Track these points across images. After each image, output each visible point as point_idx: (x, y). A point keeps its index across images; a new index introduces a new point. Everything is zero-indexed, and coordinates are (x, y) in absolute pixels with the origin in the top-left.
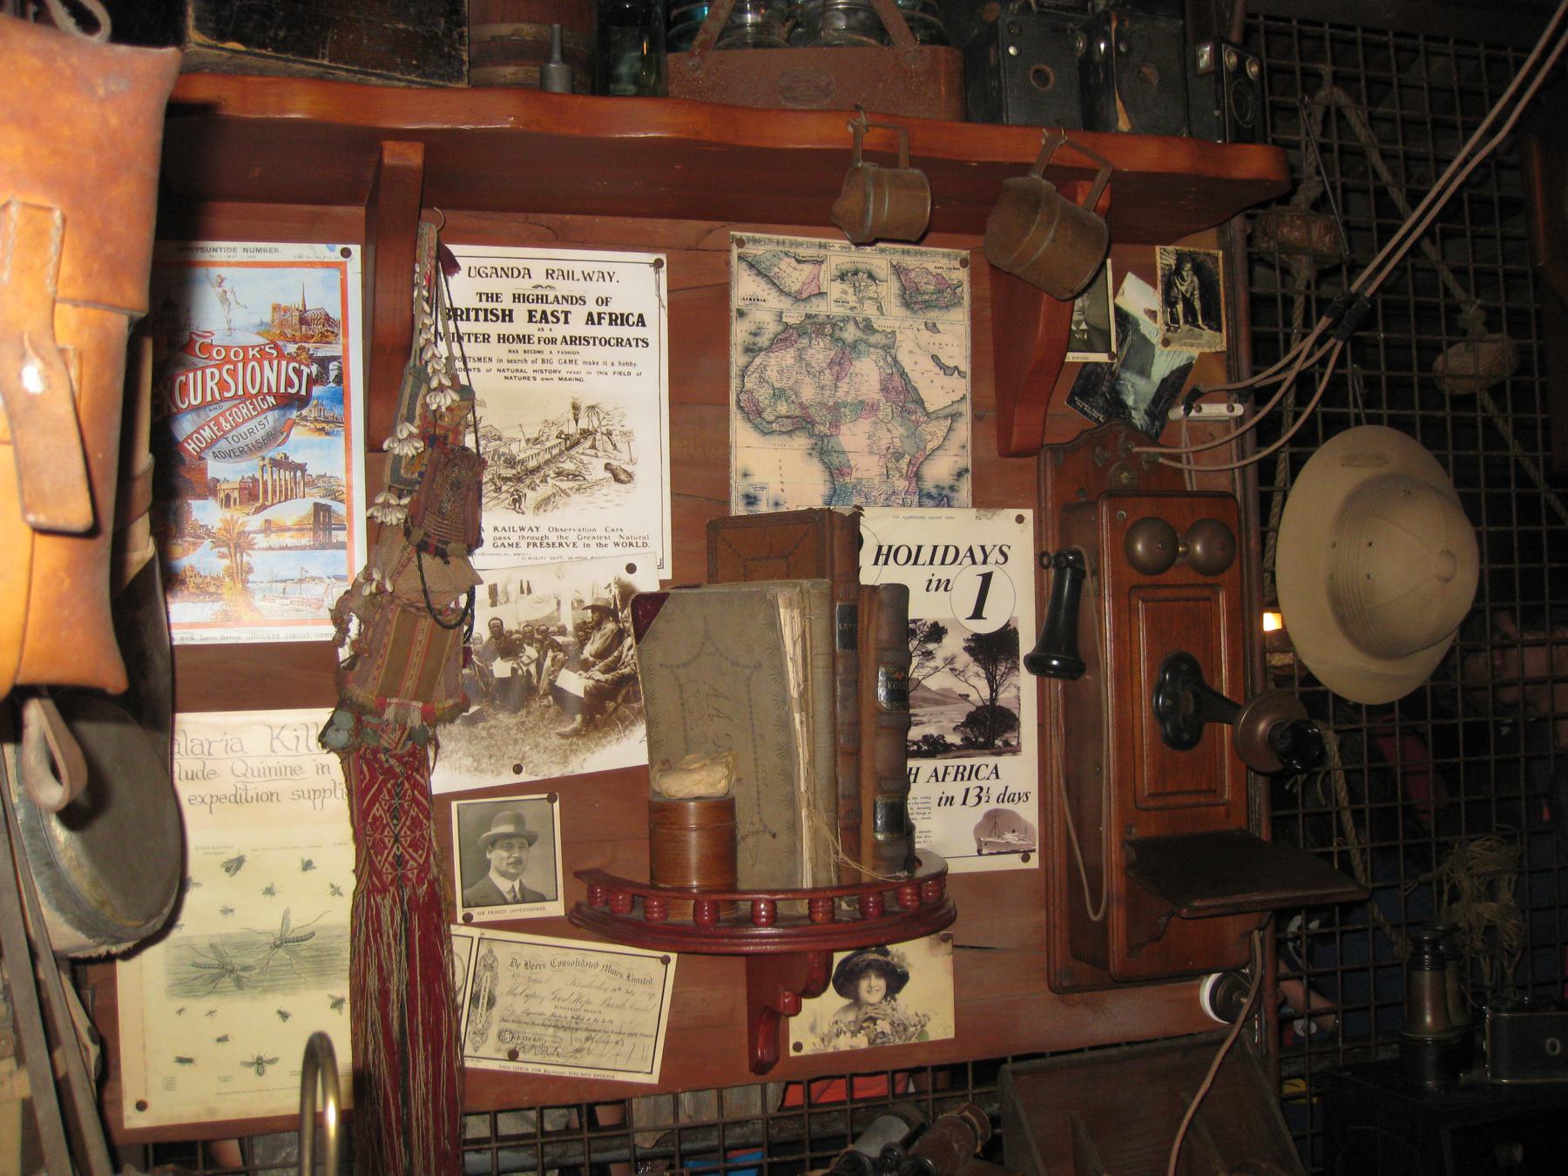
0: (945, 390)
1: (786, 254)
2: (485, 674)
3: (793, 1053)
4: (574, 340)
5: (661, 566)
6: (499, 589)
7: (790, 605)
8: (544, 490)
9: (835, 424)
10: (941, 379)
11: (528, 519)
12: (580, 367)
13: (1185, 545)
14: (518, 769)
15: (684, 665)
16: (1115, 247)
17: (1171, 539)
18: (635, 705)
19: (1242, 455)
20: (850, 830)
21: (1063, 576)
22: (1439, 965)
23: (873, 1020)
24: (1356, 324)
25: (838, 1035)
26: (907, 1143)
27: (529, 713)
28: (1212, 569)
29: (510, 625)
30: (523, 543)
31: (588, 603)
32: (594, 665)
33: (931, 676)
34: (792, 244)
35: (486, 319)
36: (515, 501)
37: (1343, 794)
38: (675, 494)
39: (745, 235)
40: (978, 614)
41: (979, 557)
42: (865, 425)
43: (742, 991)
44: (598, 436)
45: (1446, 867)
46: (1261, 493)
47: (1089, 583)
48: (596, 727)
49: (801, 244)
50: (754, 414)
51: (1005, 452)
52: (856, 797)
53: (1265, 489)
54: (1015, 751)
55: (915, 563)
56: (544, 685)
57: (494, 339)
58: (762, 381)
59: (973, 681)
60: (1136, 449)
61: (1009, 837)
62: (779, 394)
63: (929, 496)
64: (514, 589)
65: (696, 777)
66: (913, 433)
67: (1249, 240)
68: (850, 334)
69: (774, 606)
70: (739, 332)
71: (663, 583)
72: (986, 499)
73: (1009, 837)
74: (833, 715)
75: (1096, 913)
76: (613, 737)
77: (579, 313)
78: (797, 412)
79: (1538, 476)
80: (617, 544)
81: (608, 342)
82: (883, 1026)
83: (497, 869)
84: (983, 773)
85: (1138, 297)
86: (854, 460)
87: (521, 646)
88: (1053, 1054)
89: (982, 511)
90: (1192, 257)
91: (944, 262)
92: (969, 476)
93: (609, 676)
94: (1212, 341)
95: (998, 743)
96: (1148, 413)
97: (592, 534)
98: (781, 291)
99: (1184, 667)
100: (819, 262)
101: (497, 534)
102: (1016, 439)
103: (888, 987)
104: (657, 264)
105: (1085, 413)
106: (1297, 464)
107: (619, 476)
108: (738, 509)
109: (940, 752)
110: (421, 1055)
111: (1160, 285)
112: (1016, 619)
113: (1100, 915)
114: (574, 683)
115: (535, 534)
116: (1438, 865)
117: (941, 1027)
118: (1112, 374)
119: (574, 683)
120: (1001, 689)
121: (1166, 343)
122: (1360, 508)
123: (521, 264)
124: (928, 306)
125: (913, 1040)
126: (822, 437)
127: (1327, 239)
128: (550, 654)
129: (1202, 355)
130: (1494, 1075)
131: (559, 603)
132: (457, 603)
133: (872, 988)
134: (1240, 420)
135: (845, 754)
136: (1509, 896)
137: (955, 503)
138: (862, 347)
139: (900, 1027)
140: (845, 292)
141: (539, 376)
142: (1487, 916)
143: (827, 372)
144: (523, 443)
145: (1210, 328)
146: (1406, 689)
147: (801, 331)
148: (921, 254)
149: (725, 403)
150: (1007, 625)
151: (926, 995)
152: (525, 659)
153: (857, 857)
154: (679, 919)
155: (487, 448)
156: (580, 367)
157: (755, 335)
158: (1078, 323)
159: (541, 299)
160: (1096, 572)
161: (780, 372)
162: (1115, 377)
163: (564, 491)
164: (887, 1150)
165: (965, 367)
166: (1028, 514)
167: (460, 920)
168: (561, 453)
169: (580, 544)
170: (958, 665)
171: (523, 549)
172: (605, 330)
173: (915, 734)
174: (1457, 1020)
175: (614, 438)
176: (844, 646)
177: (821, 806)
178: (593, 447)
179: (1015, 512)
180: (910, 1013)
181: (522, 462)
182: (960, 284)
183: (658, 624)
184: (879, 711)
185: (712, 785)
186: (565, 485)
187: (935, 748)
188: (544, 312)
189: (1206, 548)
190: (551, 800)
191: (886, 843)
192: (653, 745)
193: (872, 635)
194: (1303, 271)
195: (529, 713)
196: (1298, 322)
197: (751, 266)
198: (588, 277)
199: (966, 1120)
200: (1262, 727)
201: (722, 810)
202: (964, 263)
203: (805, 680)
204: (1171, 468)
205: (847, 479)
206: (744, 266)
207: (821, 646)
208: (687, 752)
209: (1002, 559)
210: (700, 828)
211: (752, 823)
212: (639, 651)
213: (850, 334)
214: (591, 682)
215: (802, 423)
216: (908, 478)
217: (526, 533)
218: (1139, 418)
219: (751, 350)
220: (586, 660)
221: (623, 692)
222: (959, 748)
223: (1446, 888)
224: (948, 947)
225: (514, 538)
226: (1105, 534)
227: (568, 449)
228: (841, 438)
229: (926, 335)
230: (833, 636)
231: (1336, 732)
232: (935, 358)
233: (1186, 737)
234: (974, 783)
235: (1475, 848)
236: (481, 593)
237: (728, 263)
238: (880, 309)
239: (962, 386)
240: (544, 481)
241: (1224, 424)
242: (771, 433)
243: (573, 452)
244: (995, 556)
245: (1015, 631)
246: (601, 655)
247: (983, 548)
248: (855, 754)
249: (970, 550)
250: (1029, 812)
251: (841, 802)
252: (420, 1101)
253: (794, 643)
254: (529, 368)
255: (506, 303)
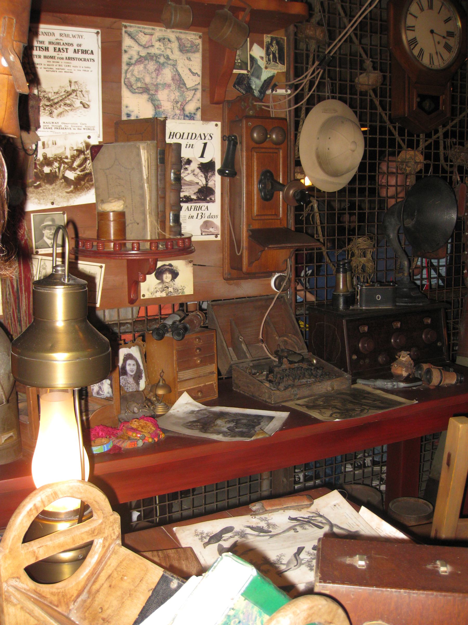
0: (193, 81)
1: (141, 31)
2: (42, 172)
3: (142, 298)
4: (69, 59)
5: (99, 137)
6: (46, 143)
7: (144, 149)
8: (60, 110)
9: (156, 91)
10: (192, 77)
11: (55, 120)
12: (72, 68)
13: (270, 135)
14: (53, 203)
15: (108, 169)
16: (251, 34)
17: (266, 133)
18: (91, 183)
19: (290, 106)
20: (163, 222)
21: (230, 143)
22: (345, 272)
23: (168, 287)
24: (327, 63)
25: (156, 292)
26: (180, 321)
27: (56, 185)
28: (278, 143)
29: (49, 155)
30: (53, 128)
31: (75, 148)
32: (77, 169)
33: (187, 176)
34: (143, 28)
35: (40, 50)
36: (50, 113)
37: (318, 221)
38: (104, 113)
39: (127, 24)
40: (202, 156)
41: (203, 137)
42: (166, 91)
43: (126, 277)
44: (78, 92)
45: (350, 246)
46: (295, 120)
47: (239, 146)
48: (78, 190)
49: (145, 28)
50: (130, 86)
51: (212, 102)
52: (164, 212)
53: (297, 119)
54: (213, 202)
55: (182, 138)
56: (61, 176)
57: (42, 57)
58: (132, 75)
59: (200, 178)
60: (255, 103)
61: (211, 230)
62: (138, 80)
63: (187, 116)
64: (50, 143)
65: (114, 204)
66: (182, 95)
67: (296, 34)
68: (162, 60)
69: (139, 149)
70: (125, 58)
71: (99, 142)
72: (205, 118)
73: (211, 230)
74: (157, 185)
75: (239, 253)
76: (83, 193)
77: (71, 49)
78: (144, 86)
79: (386, 119)
80: (84, 129)
81: (81, 60)
82: (171, 289)
83: (47, 237)
84: (203, 208)
85: (257, 52)
86: (163, 103)
87: (53, 162)
88: (224, 300)
89: (204, 122)
90: (276, 39)
91: (193, 37)
92: (200, 110)
93: (82, 173)
94: (281, 68)
95: (208, 199)
96: (260, 91)
97: (76, 125)
98: (139, 44)
99: (268, 174)
100: (152, 35)
101: (45, 124)
102: (216, 98)
103: (172, 277)
104: (98, 33)
105: (239, 91)
106: (308, 111)
107: (85, 106)
108: (124, 118)
109: (189, 201)
110: (24, 296)
111: (265, 48)
112: (214, 158)
113: (240, 253)
114: (71, 175)
115: (57, 125)
116: (348, 245)
117: (189, 290)
118: (248, 77)
119: (71, 175)
120: (209, 181)
121: (266, 68)
122: (328, 126)
123: (51, 31)
124: (188, 51)
125: (180, 294)
126: (152, 95)
127: (321, 35)
128: (63, 165)
129: (278, 73)
130: (361, 306)
131: (65, 148)
132: (32, 147)
133: (167, 277)
134: (289, 95)
135: (161, 198)
136: (370, 256)
137: (195, 119)
138: (166, 65)
139: (176, 290)
140: (160, 46)
141: (58, 70)
142: (363, 262)
143: (154, 73)
144: (53, 94)
145: (281, 64)
146: (340, 187)
147: (145, 58)
148: (186, 33)
149: (120, 82)
150: (212, 160)
151: (185, 279)
152: (54, 167)
153: (164, 231)
154: (108, 250)
155: (42, 95)
156: (72, 68)
157: (130, 59)
158: (238, 60)
159: (58, 44)
160: (241, 143)
161: (139, 72)
162: (249, 79)
163: (66, 110)
164: (174, 323)
165: (200, 73)
166: (219, 124)
167: (34, 253)
168: (66, 97)
169: (72, 128)
170: (196, 173)
171: (53, 130)
172: (80, 55)
173: (182, 195)
174: (350, 290)
175: (83, 93)
176: (161, 163)
177: (153, 214)
178: (76, 96)
179: (214, 123)
180: (179, 286)
181: (53, 100)
182: (199, 45)
183: (99, 155)
184: (172, 184)
185: (119, 207)
186: (67, 108)
187: (188, 200)
188: (59, 48)
189: (276, 136)
190: (64, 214)
191: (174, 227)
192: (97, 196)
193: (170, 160)
194: (313, 46)
195: (56, 185)
196: (310, 63)
197: (129, 35)
198: (74, 37)
199: (198, 315)
200: (291, 192)
201: (121, 216)
202: (200, 37)
203: (148, 174)
204: (266, 110)
205: (160, 110)
206: (127, 35)
207: (154, 163)
208: (109, 197)
209: (210, 138)
210: (114, 221)
211: (131, 220)
212: (93, 165)
213: (162, 60)
214: (76, 175)
215: (145, 90)
216: (180, 110)
217: (54, 124)
218: (256, 93)
219: (129, 64)
220: (75, 168)
221: (87, 178)
222: (195, 200)
223: (350, 253)
224: (191, 264)
225: (50, 126)
226: (244, 130)
227: (68, 96)
228: (158, 95)
229: (187, 62)
230: (157, 160)
231: (317, 200)
232: (190, 70)
233: (268, 197)
234: (200, 212)
235: (360, 240)
236: (40, 144)
237: (121, 34)
238: (172, 52)
239: (198, 80)
240: (60, 107)
241: (284, 96)
242: (135, 93)
243: (70, 97)
244: (208, 137)
245: (214, 162)
246: (79, 166)
247: (204, 134)
248: (164, 198)
249: (200, 135)
250: (217, 222)
251: (159, 213)
252: (24, 312)
253: (145, 161)
254: (54, 68)
255: (47, 45)
